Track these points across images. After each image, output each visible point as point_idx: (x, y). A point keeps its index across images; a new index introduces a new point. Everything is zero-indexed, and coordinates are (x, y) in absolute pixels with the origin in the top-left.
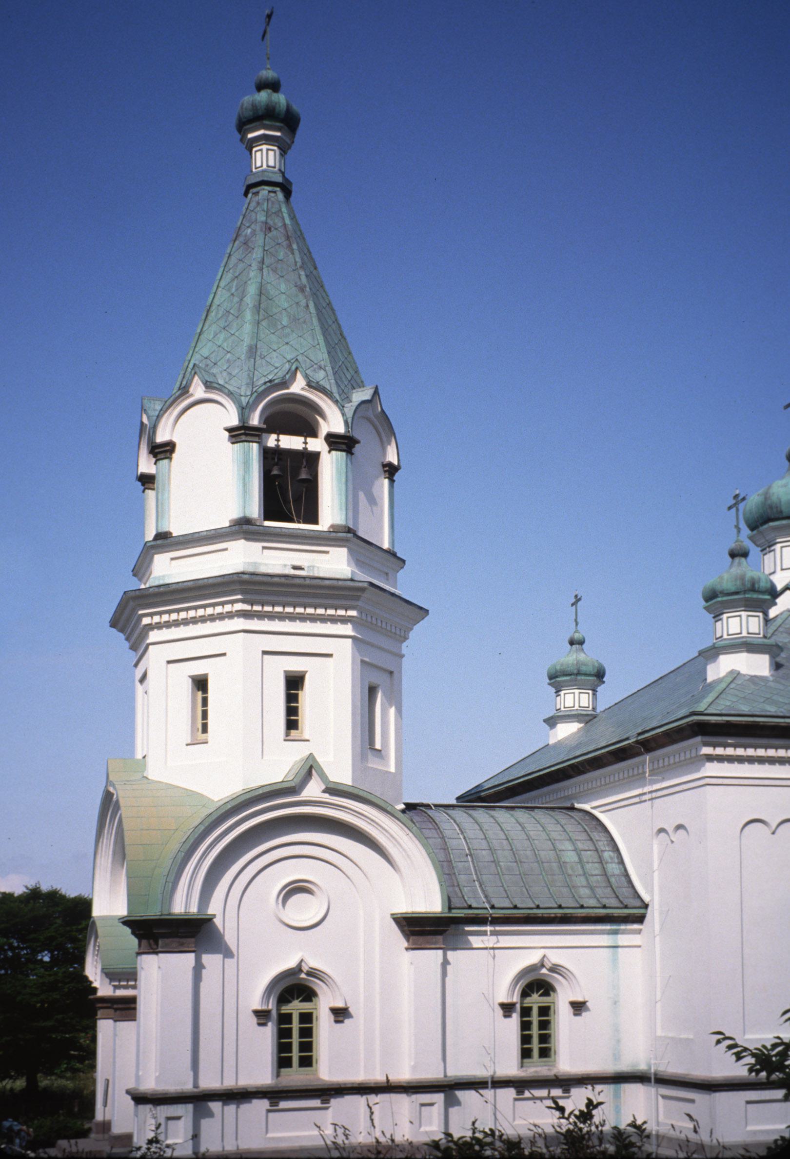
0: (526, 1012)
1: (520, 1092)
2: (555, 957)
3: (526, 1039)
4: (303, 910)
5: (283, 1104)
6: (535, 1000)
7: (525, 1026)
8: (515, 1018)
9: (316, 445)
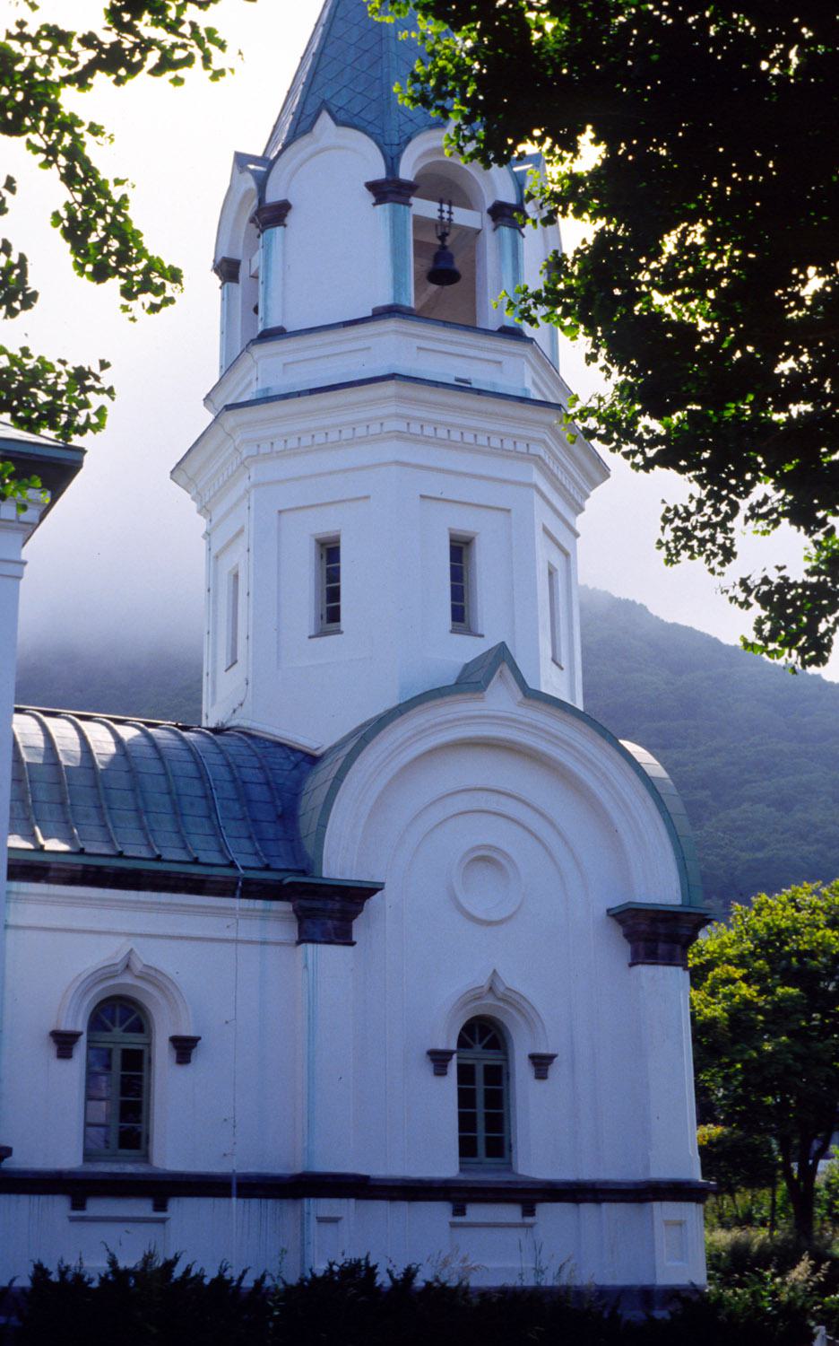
0: (465, 1074)
1: (459, 1211)
2: (153, 955)
3: (466, 1122)
4: (484, 898)
5: (96, 1207)
6: (481, 1057)
7: (465, 1098)
8: (449, 1085)
9: (462, 217)
